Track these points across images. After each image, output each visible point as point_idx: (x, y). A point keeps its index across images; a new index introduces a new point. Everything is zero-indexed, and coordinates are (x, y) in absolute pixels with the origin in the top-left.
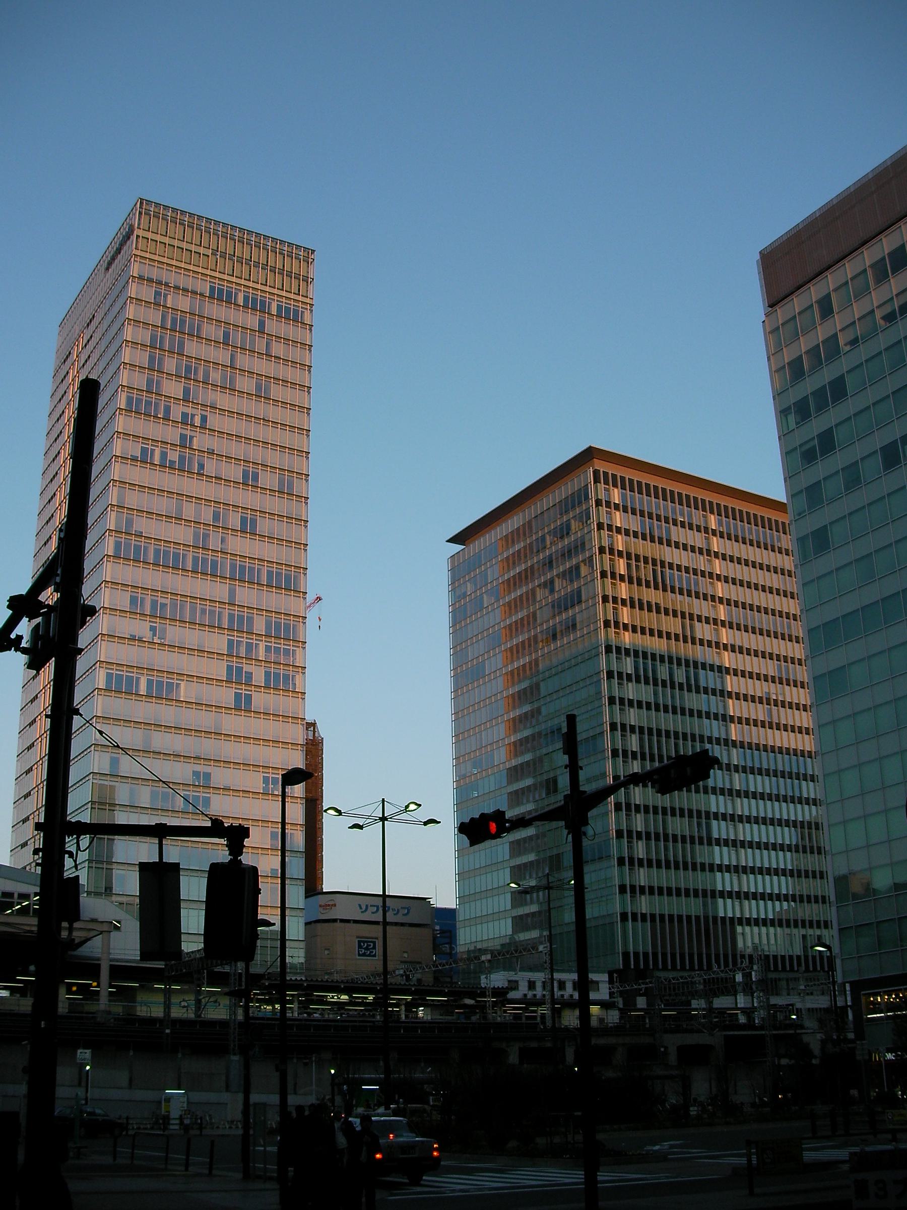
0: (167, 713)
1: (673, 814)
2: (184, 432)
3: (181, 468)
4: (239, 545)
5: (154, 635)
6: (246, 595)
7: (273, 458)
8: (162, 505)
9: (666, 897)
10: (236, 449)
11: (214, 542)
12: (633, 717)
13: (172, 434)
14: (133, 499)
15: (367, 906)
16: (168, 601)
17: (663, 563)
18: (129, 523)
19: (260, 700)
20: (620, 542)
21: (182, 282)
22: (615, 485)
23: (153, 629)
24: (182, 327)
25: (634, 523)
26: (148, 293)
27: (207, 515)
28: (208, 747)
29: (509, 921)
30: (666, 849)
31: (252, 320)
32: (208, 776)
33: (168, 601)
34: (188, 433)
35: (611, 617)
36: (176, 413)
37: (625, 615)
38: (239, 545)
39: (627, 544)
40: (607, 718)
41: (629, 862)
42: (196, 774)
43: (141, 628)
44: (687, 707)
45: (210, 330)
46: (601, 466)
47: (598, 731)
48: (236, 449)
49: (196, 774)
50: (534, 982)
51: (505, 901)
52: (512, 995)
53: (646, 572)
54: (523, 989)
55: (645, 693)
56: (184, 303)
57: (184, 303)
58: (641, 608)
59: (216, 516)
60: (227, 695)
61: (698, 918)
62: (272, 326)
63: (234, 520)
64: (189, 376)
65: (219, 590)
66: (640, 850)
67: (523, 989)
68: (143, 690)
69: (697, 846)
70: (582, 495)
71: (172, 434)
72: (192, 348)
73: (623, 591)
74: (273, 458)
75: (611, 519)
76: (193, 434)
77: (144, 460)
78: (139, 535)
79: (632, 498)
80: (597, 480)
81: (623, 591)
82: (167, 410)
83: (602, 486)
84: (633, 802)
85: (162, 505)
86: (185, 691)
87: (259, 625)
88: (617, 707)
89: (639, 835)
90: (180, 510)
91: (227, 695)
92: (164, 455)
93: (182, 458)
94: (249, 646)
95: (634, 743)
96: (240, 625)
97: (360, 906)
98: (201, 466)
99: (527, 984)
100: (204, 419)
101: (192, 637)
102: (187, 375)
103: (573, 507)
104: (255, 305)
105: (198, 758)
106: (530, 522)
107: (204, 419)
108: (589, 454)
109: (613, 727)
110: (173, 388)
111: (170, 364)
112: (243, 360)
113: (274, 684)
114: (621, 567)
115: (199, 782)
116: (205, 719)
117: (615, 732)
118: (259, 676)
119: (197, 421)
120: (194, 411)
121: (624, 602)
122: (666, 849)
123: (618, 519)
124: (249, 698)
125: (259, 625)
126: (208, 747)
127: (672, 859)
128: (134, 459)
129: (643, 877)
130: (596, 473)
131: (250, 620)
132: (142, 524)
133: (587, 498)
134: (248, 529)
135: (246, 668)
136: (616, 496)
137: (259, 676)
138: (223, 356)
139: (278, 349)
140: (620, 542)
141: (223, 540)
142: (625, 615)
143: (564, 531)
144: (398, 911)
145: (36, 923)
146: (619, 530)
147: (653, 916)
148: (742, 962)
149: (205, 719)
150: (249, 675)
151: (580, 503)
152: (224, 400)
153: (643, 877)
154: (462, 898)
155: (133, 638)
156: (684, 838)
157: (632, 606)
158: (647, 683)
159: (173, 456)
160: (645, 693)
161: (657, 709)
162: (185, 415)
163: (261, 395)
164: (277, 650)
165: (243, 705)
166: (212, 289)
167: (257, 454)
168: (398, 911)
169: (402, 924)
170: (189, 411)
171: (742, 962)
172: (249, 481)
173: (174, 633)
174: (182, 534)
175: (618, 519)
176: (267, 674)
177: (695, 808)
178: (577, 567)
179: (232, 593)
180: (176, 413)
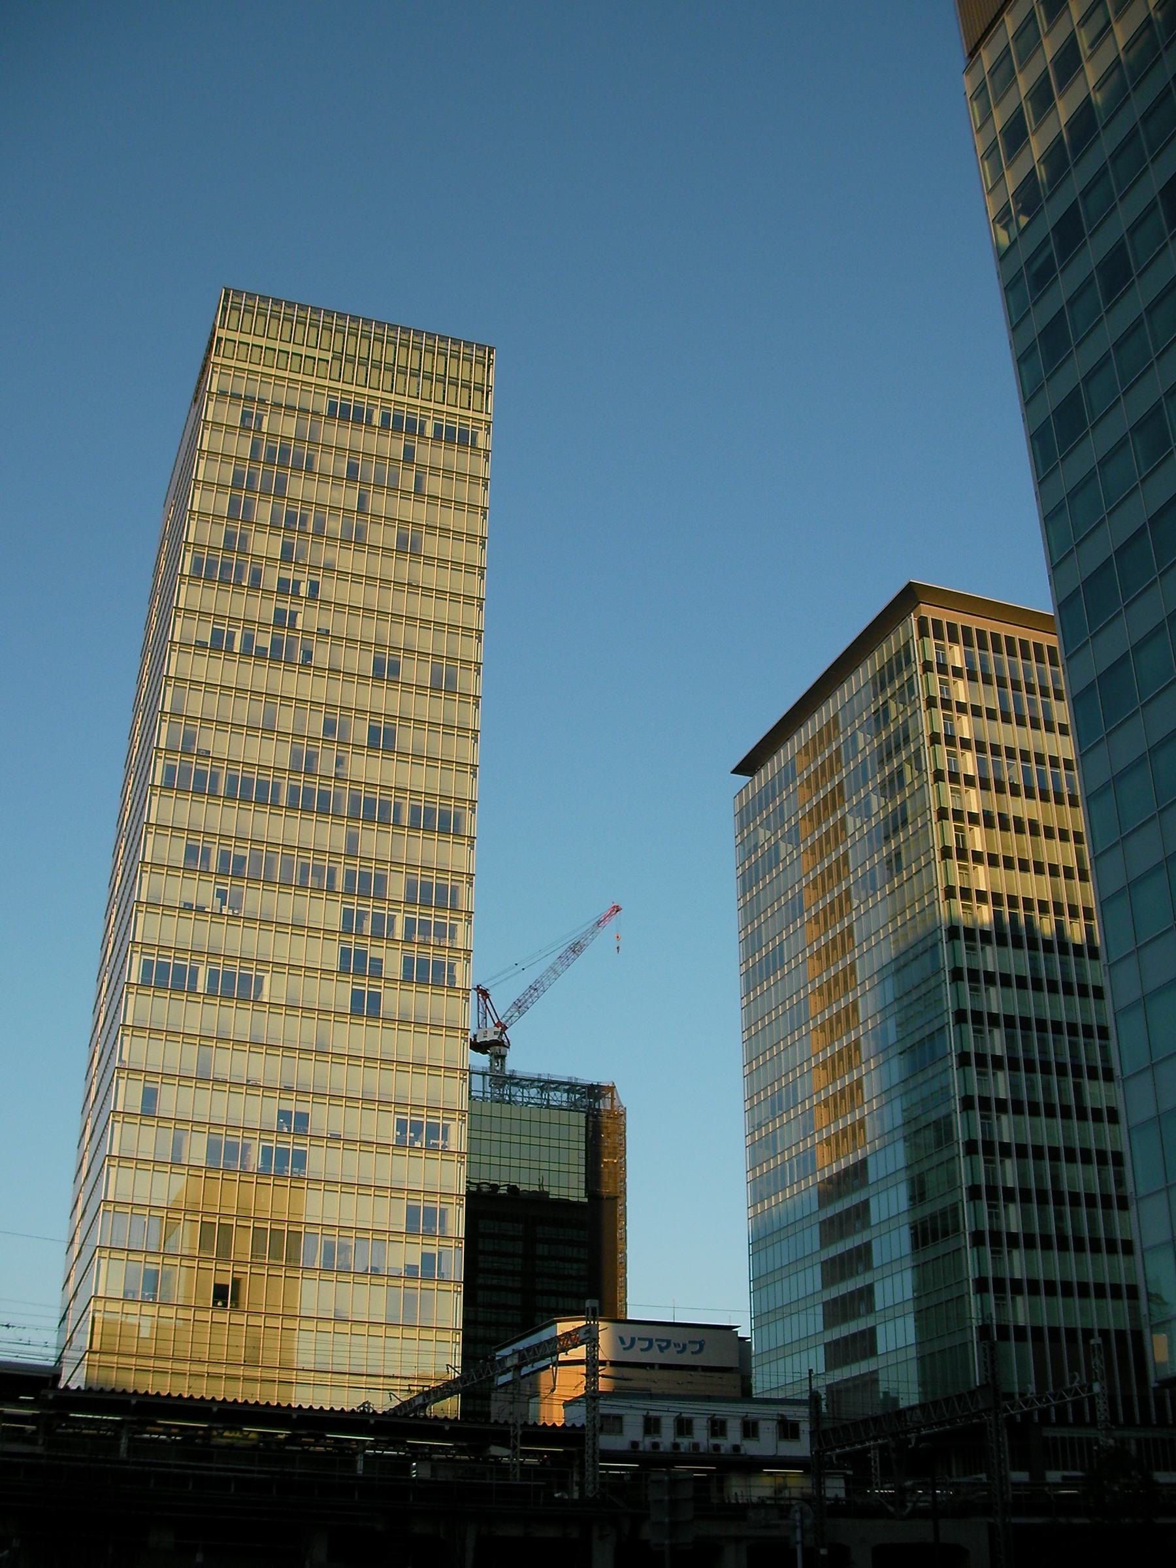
0: (239, 1020)
1: (1071, 1158)
2: (281, 606)
3: (277, 655)
4: (367, 769)
5: (223, 903)
6: (375, 842)
7: (425, 640)
8: (243, 710)
9: (1060, 1299)
10: (368, 629)
11: (326, 764)
12: (995, 1000)
13: (263, 609)
14: (195, 704)
15: (633, 1340)
16: (247, 853)
17: (1040, 759)
18: (189, 739)
19: (393, 1000)
20: (965, 727)
21: (283, 396)
22: (953, 639)
23: (221, 894)
24: (286, 459)
25: (989, 698)
26: (232, 414)
27: (316, 725)
28: (307, 1072)
29: (821, 1350)
30: (1059, 1217)
31: (394, 446)
32: (303, 1118)
33: (247, 853)
34: (287, 607)
35: (952, 843)
36: (271, 579)
37: (977, 839)
38: (367, 769)
39: (975, 729)
40: (949, 1004)
41: (995, 1240)
42: (284, 1115)
43: (204, 892)
44: (1090, 983)
45: (326, 462)
46: (929, 612)
47: (936, 1025)
48: (368, 629)
49: (284, 1115)
50: (657, 1420)
51: (815, 1319)
52: (607, 1442)
53: (1013, 772)
54: (633, 1431)
55: (1017, 962)
56: (288, 426)
57: (288, 426)
58: (1004, 827)
59: (329, 727)
60: (340, 993)
61: (1120, 1334)
62: (425, 453)
63: (360, 732)
64: (292, 526)
65: (329, 835)
66: (1013, 1219)
67: (633, 1431)
68: (202, 985)
69: (1116, 1212)
70: (904, 657)
71: (263, 609)
72: (297, 487)
73: (973, 801)
74: (425, 640)
75: (948, 693)
76: (295, 608)
77: (219, 644)
78: (205, 755)
79: (983, 659)
80: (923, 633)
81: (973, 801)
82: (256, 576)
83: (931, 642)
84: (996, 1138)
85: (243, 710)
86: (272, 988)
87: (397, 887)
88: (966, 985)
89: (1009, 1194)
90: (270, 717)
91: (340, 993)
92: (248, 640)
93: (276, 643)
94: (378, 919)
95: (997, 1042)
96: (367, 885)
97: (621, 1339)
98: (308, 655)
99: (641, 1420)
100: (314, 587)
101: (284, 905)
102: (291, 522)
103: (891, 679)
104: (395, 424)
105: (289, 1090)
106: (836, 716)
107: (314, 587)
108: (910, 596)
109: (960, 1016)
110: (266, 544)
111: (264, 511)
112: (379, 503)
113: (427, 974)
114: (969, 763)
115: (289, 1129)
116: (303, 1031)
117: (963, 1026)
118: (393, 964)
119: (304, 590)
120: (298, 577)
121: (973, 819)
122: (1059, 1217)
123: (961, 691)
124: (375, 998)
125: (397, 887)
126: (307, 1072)
127: (1070, 1233)
128: (201, 645)
129: (1018, 1265)
130: (922, 622)
131: (381, 880)
132: (208, 740)
133: (908, 661)
134: (381, 740)
135: (373, 953)
136: (956, 656)
137: (393, 964)
138: (348, 497)
139: (434, 485)
140: (965, 727)
141: (340, 762)
142: (977, 839)
143: (881, 716)
144: (685, 1346)
145: (827, 1490)
146: (962, 708)
147: (1037, 1331)
148: (1073, 1379)
149: (303, 1031)
150: (377, 963)
151: (900, 671)
152: (346, 559)
153: (1018, 1265)
154: (760, 1318)
155: (188, 907)
156: (1091, 1198)
157: (989, 824)
158: (1017, 944)
159: (264, 640)
160: (1017, 962)
161: (1037, 986)
162: (283, 582)
163: (407, 547)
164: (425, 924)
165: (365, 1007)
166: (333, 406)
167: (399, 635)
168: (685, 1346)
169: (693, 1368)
170: (289, 575)
171: (1073, 1379)
172: (385, 671)
173: (255, 899)
174: (271, 753)
175: (961, 691)
176: (408, 962)
177: (1109, 1149)
178: (900, 773)
179: (352, 840)
180: (271, 579)
